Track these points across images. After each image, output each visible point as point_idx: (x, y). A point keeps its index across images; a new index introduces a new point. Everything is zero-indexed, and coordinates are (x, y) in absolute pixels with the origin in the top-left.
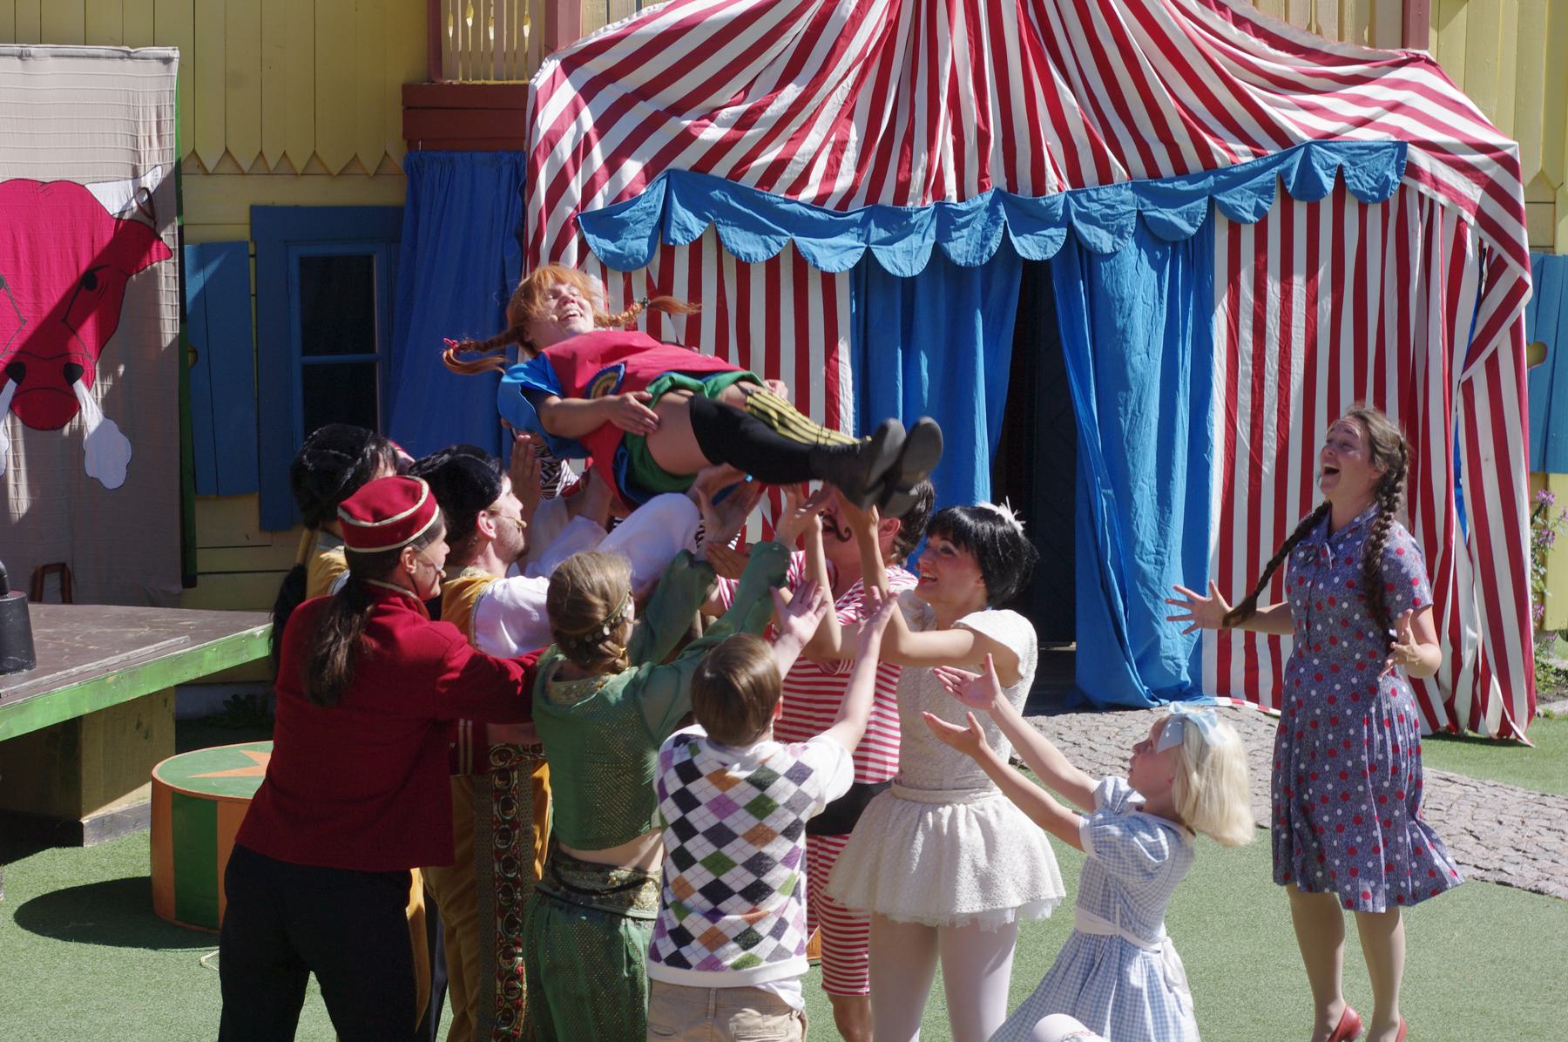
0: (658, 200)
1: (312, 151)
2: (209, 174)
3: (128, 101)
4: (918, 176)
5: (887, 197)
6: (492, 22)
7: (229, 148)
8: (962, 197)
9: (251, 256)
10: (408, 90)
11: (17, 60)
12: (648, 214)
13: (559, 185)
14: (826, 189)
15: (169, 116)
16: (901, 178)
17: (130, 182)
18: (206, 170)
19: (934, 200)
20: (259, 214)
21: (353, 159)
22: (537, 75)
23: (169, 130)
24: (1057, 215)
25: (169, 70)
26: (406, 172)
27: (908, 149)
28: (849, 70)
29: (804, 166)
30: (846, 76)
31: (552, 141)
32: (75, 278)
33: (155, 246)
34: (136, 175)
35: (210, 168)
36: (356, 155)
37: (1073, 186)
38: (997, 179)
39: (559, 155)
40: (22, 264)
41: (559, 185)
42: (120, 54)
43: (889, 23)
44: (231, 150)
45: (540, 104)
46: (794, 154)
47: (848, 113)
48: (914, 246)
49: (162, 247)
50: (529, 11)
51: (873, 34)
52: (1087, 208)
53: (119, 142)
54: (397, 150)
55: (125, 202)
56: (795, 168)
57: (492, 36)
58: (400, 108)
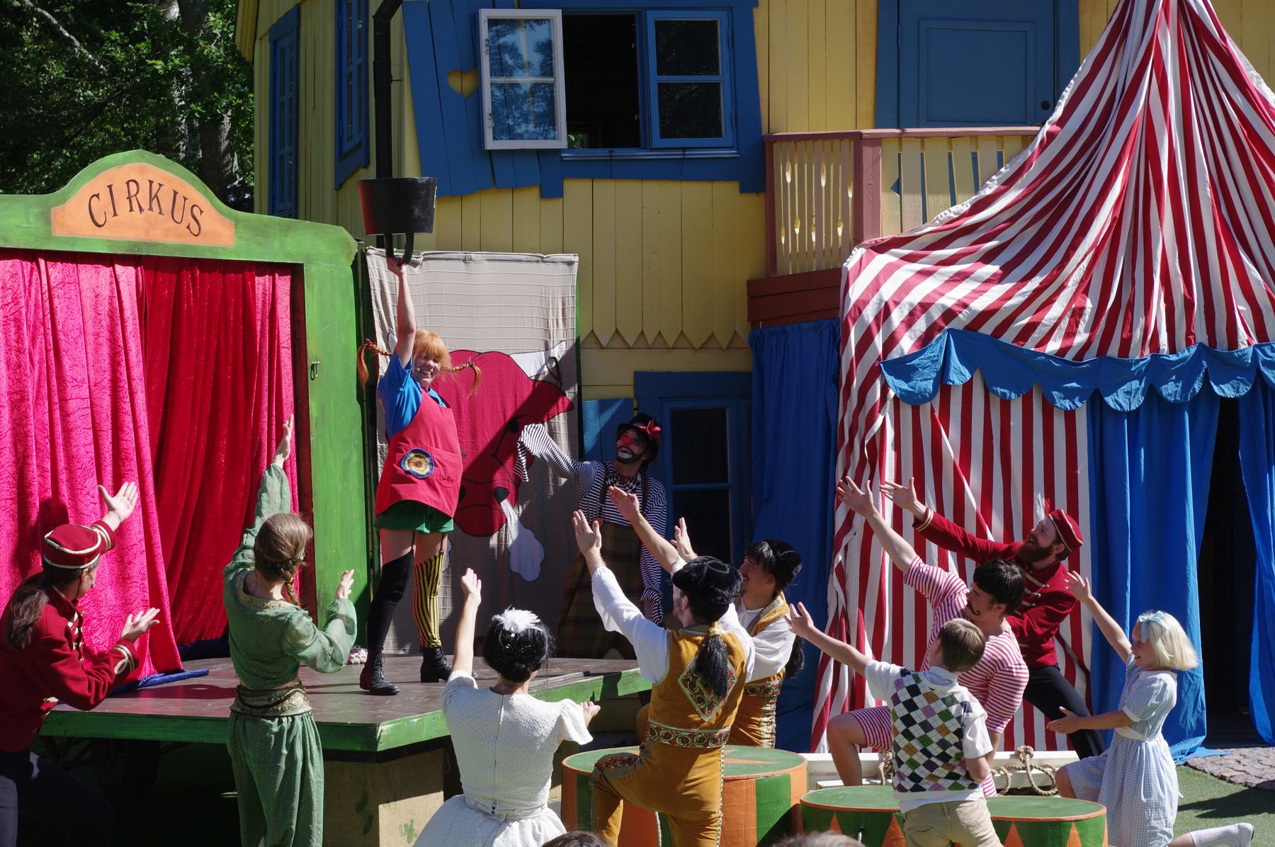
0: (940, 352)
1: (680, 332)
2: (603, 348)
3: (542, 293)
4: (1138, 334)
5: (1113, 351)
6: (814, 228)
7: (618, 328)
8: (1173, 350)
9: (635, 409)
10: (752, 284)
11: (462, 263)
12: (933, 361)
13: (866, 340)
14: (1068, 343)
15: (571, 304)
16: (1125, 336)
17: (543, 353)
18: (601, 345)
19: (1151, 352)
20: (641, 378)
21: (710, 337)
22: (848, 260)
23: (571, 314)
24: (1247, 363)
25: (571, 270)
26: (751, 345)
27: (1130, 314)
28: (1086, 256)
29: (1049, 328)
30: (1083, 259)
31: (859, 307)
32: (502, 424)
33: (560, 400)
34: (547, 349)
35: (604, 344)
36: (713, 334)
37: (1259, 340)
38: (1201, 336)
39: (866, 318)
40: (463, 413)
41: (866, 340)
42: (536, 258)
43: (1114, 219)
44: (620, 331)
45: (851, 281)
46: (1043, 319)
47: (1084, 288)
48: (1133, 388)
49: (566, 401)
50: (842, 217)
51: (1103, 228)
52: (1271, 357)
53: (535, 324)
54: (743, 328)
55: (539, 368)
56: (1043, 329)
57: (814, 239)
58: (745, 299)
